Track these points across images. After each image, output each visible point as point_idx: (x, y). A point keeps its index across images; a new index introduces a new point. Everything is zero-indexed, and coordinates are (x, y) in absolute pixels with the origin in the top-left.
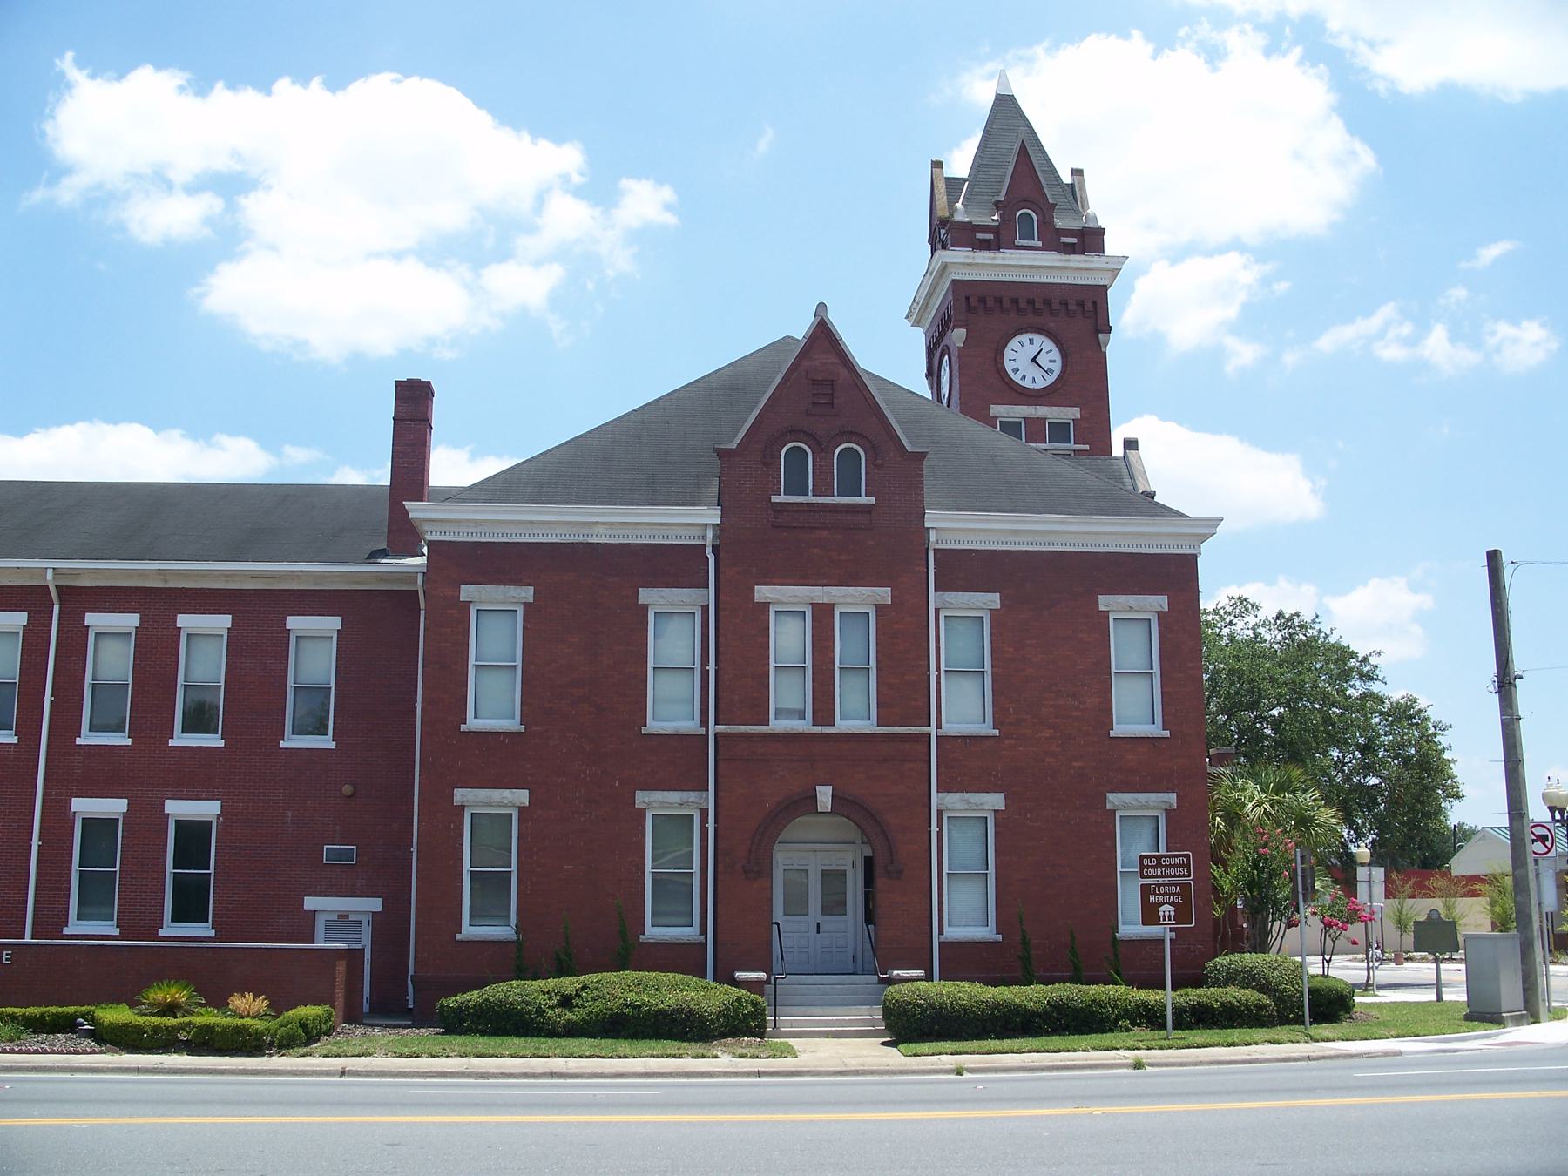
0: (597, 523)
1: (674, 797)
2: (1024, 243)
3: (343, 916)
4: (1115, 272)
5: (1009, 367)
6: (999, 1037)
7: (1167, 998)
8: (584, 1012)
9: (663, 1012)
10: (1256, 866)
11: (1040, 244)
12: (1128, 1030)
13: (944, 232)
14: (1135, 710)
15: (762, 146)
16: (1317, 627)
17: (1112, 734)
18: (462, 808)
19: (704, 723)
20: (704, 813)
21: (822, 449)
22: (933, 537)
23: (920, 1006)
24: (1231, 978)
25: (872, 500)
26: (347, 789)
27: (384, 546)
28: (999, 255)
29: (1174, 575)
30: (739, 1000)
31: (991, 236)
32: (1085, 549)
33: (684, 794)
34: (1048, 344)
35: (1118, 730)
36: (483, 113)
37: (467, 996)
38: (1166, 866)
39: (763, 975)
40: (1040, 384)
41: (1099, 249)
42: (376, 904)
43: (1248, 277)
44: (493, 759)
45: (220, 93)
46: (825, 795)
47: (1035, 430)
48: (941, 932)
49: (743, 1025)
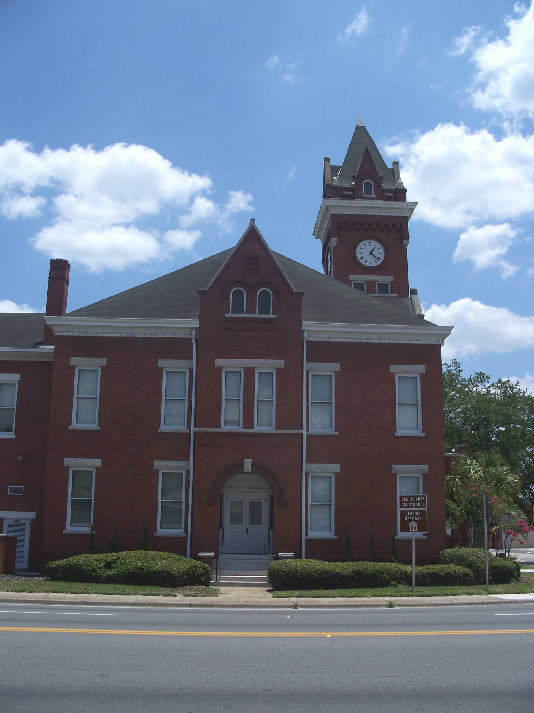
0: (138, 327)
1: (173, 464)
2: (367, 196)
3: (17, 521)
4: (412, 210)
5: (359, 256)
6: (326, 588)
7: (413, 569)
8: (117, 570)
9: (154, 572)
10: (470, 503)
11: (375, 196)
12: (395, 586)
13: (330, 191)
14: (408, 422)
15: (291, 175)
16: (518, 387)
17: (396, 435)
18: (68, 467)
19: (189, 427)
20: (188, 472)
21: (251, 292)
22: (306, 335)
23: (285, 571)
24: (453, 560)
25: (275, 316)
26: (20, 458)
27: (42, 340)
28: (354, 201)
29: (430, 354)
30: (195, 567)
31: (350, 193)
32: (384, 342)
33: (178, 462)
34: (378, 245)
35: (399, 432)
36: (167, 161)
37: (60, 562)
38: (413, 502)
39: (212, 554)
40: (374, 264)
41: (404, 199)
42: (32, 515)
43: (512, 234)
44: (86, 444)
45: (47, 152)
46: (248, 464)
47: (371, 287)
48: (306, 534)
49: (198, 580)
